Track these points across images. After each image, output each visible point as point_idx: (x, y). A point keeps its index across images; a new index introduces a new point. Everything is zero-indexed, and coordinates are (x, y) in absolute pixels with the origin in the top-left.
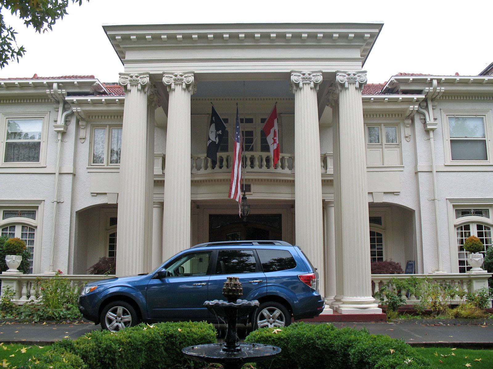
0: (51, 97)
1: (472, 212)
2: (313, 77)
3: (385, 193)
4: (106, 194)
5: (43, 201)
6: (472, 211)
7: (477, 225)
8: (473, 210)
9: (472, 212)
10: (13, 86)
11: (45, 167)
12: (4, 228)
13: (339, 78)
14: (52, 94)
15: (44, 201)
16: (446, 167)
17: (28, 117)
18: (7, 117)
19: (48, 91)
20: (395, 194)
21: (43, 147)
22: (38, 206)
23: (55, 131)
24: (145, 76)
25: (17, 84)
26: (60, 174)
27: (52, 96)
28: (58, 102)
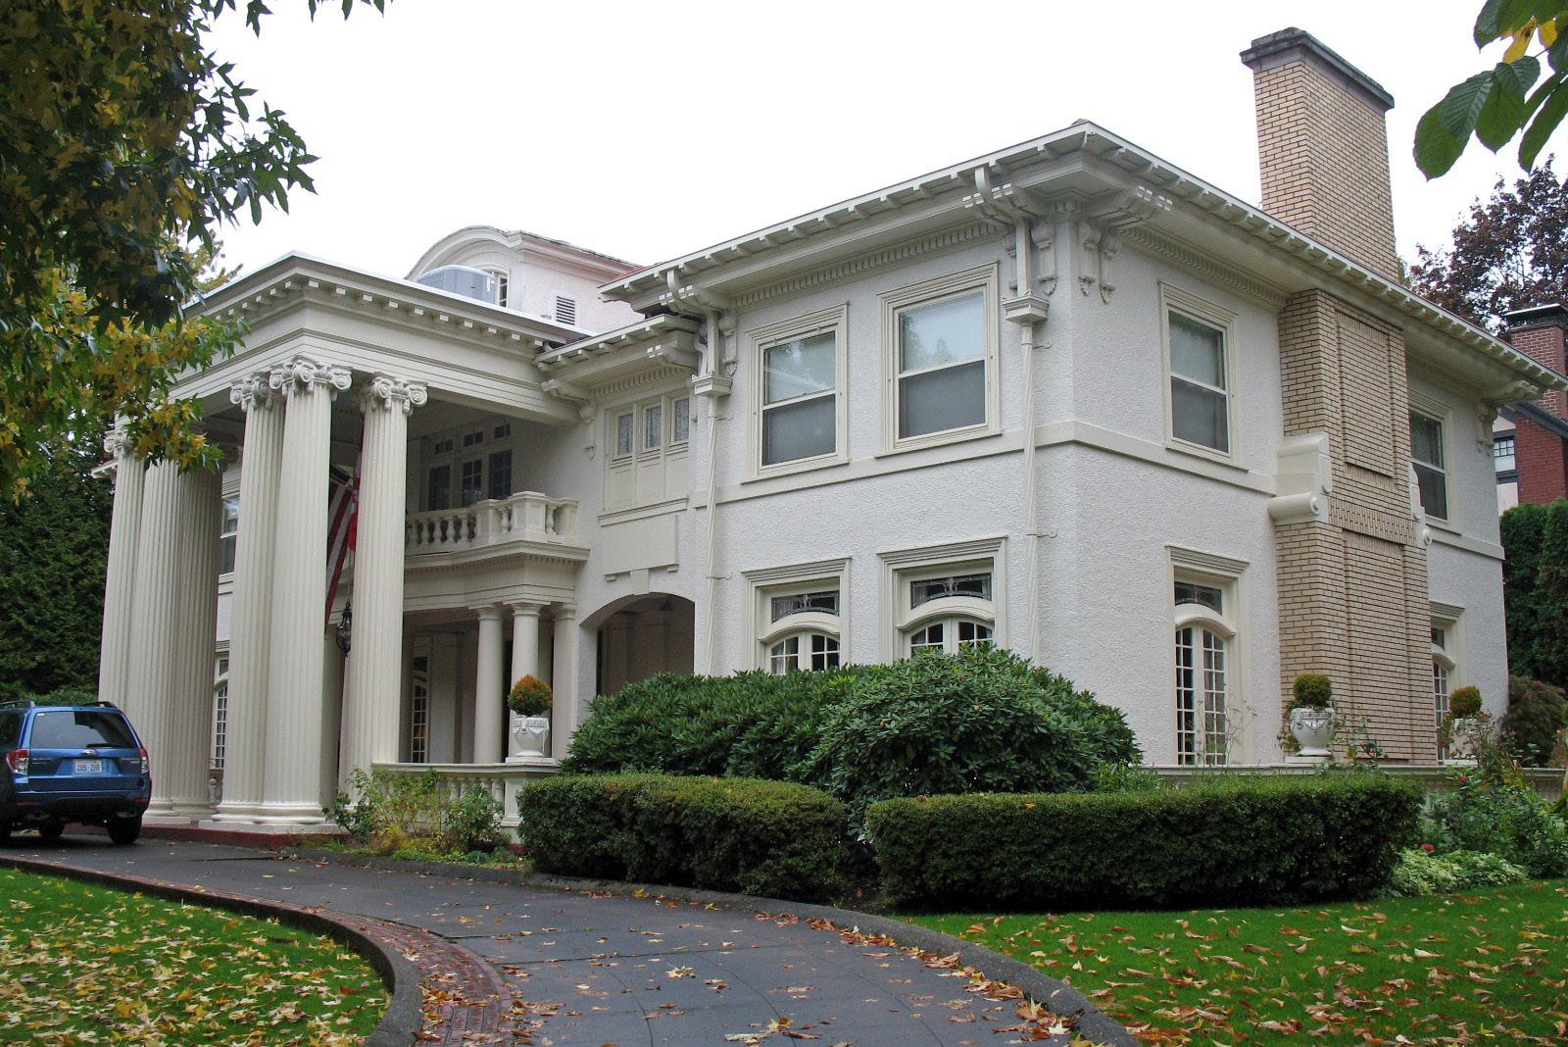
0: (1012, 207)
2: (334, 376)
3: (652, 570)
4: (628, 573)
5: (847, 562)
8: (954, 578)
10: (945, 188)
11: (847, 464)
12: (915, 633)
13: (378, 386)
14: (980, 206)
16: (880, 462)
17: (954, 289)
18: (895, 305)
22: (838, 577)
23: (1009, 319)
24: (344, 372)
25: (956, 179)
26: (1038, 448)
27: (985, 214)
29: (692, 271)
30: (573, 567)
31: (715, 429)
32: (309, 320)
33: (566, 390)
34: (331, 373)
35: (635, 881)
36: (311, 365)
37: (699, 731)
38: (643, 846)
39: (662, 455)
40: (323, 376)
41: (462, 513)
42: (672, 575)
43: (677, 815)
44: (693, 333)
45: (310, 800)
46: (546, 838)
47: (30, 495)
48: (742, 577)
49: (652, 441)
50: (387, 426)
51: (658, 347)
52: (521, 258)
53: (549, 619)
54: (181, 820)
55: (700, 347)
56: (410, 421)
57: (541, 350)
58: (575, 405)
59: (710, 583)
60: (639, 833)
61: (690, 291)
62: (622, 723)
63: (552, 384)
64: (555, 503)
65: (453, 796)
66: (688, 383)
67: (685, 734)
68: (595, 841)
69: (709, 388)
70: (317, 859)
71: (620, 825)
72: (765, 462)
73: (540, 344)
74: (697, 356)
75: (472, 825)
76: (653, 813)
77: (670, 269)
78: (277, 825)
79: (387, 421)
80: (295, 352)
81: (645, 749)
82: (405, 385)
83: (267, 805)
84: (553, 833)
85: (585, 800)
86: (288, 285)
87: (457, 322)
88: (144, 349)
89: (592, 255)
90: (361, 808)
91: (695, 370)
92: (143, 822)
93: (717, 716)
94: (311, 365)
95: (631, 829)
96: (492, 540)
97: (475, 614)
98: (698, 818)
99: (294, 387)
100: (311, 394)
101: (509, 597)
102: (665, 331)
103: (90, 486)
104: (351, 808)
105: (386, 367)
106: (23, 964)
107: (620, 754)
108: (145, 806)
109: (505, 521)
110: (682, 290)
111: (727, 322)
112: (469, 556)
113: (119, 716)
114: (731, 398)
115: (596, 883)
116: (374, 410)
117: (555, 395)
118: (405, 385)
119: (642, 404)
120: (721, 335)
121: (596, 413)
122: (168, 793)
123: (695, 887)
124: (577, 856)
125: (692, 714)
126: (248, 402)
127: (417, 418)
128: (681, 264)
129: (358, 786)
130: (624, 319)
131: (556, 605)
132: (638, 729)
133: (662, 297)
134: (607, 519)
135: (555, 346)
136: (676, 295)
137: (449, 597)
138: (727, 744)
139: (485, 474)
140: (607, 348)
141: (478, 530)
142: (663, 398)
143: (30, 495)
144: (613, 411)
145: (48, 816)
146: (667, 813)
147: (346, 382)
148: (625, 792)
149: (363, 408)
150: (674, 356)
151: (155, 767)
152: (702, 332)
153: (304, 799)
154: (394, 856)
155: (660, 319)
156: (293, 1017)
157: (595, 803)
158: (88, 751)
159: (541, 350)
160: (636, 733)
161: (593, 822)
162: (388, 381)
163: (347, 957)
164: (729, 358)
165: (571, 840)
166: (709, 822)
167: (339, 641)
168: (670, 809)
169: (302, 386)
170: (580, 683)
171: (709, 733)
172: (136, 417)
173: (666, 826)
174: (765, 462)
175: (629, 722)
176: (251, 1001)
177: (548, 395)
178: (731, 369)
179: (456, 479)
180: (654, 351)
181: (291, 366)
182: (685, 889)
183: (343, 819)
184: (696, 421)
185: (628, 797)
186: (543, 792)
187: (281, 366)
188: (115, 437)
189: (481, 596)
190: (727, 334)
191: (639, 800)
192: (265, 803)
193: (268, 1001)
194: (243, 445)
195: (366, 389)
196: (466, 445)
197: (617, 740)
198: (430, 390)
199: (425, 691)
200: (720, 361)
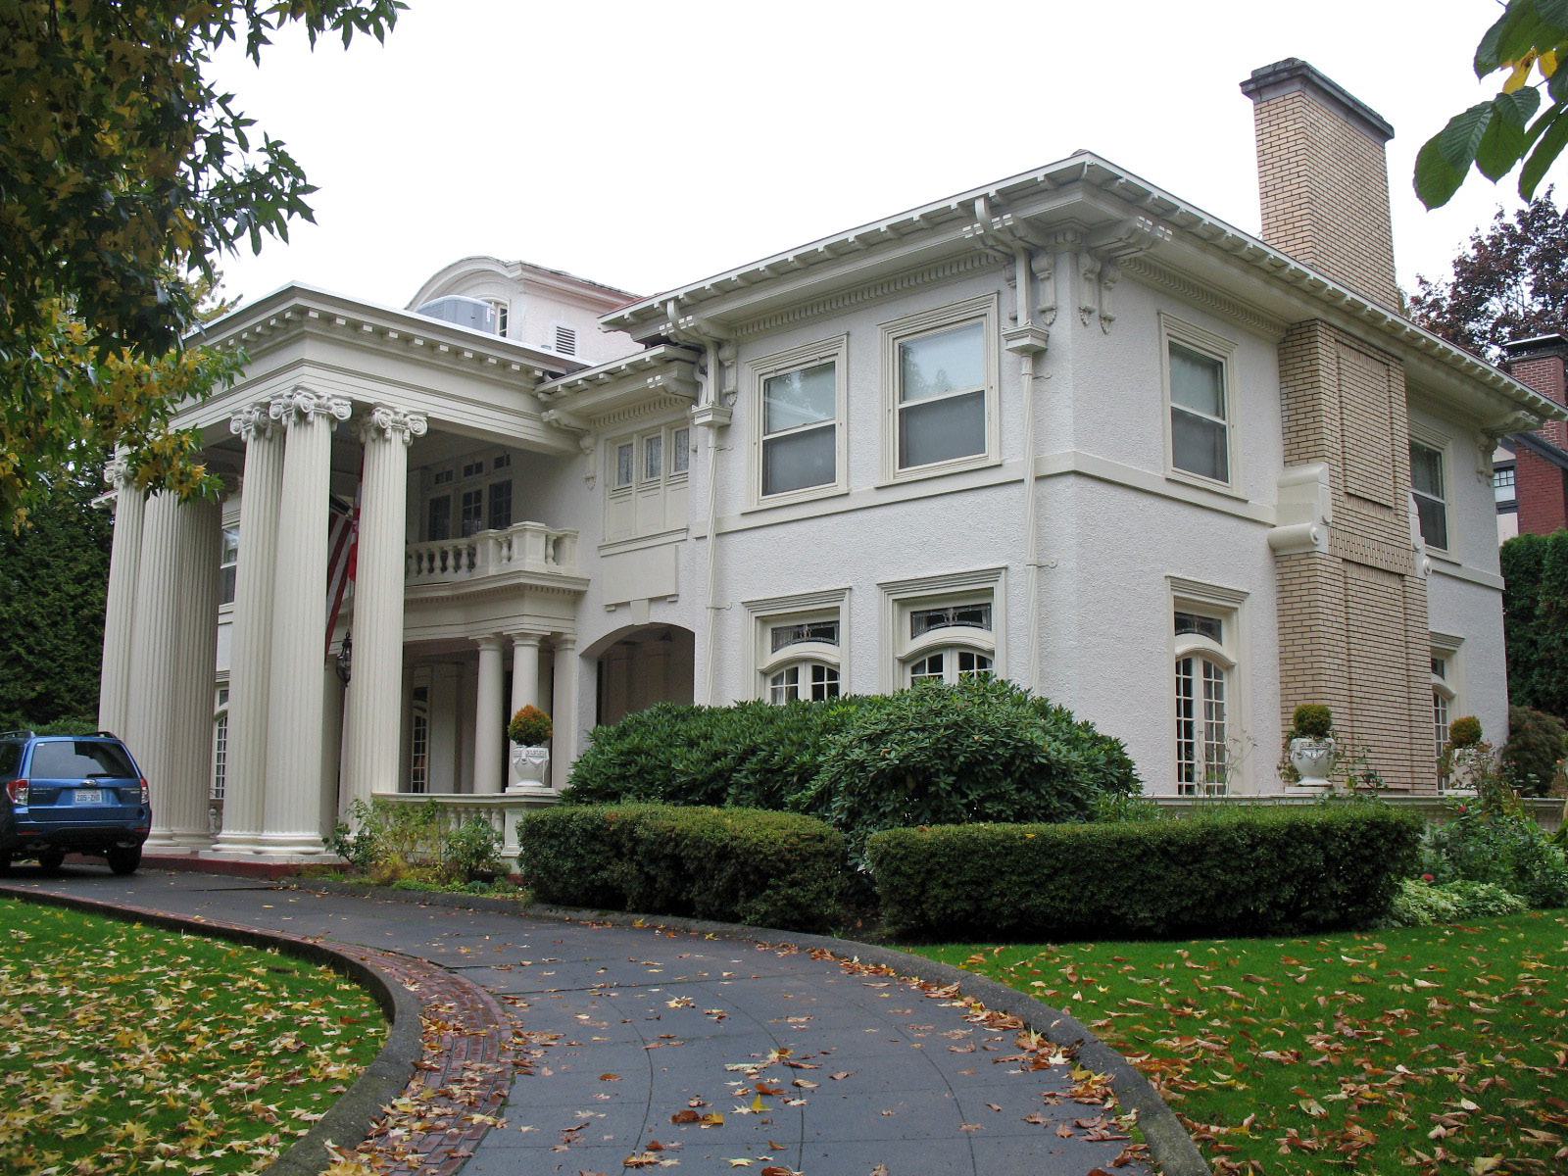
0: (1011, 238)
1: (951, 617)
3: (652, 600)
4: (628, 603)
5: (847, 592)
6: (951, 614)
7: (961, 655)
9: (951, 617)
13: (378, 416)
15: (1006, 568)
19: (967, 231)
20: (669, 599)
21: (991, 403)
23: (1009, 350)
26: (1038, 479)
28: (1011, 259)
29: (692, 301)
30: (573, 597)
32: (309, 351)
33: (566, 420)
34: (331, 403)
35: (635, 911)
36: (311, 395)
37: (699, 761)
40: (324, 407)
41: (462, 543)
42: (672, 606)
43: (677, 845)
44: (693, 363)
45: (310, 830)
46: (546, 868)
47: (30, 525)
49: (652, 471)
51: (658, 378)
52: (521, 288)
53: (549, 649)
55: (700, 377)
56: (410, 451)
57: (541, 380)
58: (575, 435)
59: (710, 613)
60: (639, 864)
62: (622, 753)
63: (552, 414)
64: (555, 533)
65: (453, 827)
67: (685, 764)
68: (595, 871)
69: (709, 418)
71: (620, 856)
72: (765, 492)
74: (697, 386)
75: (472, 855)
76: (653, 843)
77: (670, 300)
78: (277, 855)
82: (405, 416)
83: (267, 835)
84: (553, 863)
85: (584, 830)
87: (457, 352)
89: (592, 285)
90: (361, 838)
92: (143, 852)
93: (717, 746)
94: (311, 395)
96: (492, 571)
99: (294, 418)
100: (311, 424)
101: (510, 627)
102: (664, 362)
103: (90, 517)
104: (351, 838)
106: (23, 995)
107: (621, 784)
109: (505, 551)
110: (682, 321)
112: (477, 585)
113: (119, 746)
115: (596, 913)
116: (374, 441)
119: (642, 434)
120: (721, 365)
121: (596, 444)
122: (168, 823)
123: (695, 917)
125: (692, 744)
126: (248, 432)
127: (417, 449)
128: (681, 294)
130: (624, 349)
133: (662, 328)
135: (555, 376)
136: (676, 325)
137: (449, 627)
138: (727, 775)
140: (607, 378)
141: (478, 560)
143: (30, 525)
146: (667, 843)
147: (345, 412)
149: (362, 439)
150: (674, 387)
153: (304, 830)
154: (394, 886)
155: (660, 350)
156: (293, 1047)
157: (595, 833)
158: (88, 781)
159: (541, 380)
160: (636, 764)
161: (593, 852)
163: (347, 987)
164: (729, 389)
165: (571, 870)
167: (339, 672)
168: (670, 839)
169: (302, 416)
171: (709, 764)
173: (666, 856)
174: (765, 492)
175: (629, 752)
176: (251, 1031)
177: (548, 425)
178: (731, 400)
179: (455, 508)
184: (696, 451)
185: (628, 827)
186: (543, 822)
187: (281, 396)
188: (115, 467)
189: (482, 626)
193: (268, 1031)
195: (366, 419)
197: (617, 770)
198: (430, 420)
200: (720, 391)
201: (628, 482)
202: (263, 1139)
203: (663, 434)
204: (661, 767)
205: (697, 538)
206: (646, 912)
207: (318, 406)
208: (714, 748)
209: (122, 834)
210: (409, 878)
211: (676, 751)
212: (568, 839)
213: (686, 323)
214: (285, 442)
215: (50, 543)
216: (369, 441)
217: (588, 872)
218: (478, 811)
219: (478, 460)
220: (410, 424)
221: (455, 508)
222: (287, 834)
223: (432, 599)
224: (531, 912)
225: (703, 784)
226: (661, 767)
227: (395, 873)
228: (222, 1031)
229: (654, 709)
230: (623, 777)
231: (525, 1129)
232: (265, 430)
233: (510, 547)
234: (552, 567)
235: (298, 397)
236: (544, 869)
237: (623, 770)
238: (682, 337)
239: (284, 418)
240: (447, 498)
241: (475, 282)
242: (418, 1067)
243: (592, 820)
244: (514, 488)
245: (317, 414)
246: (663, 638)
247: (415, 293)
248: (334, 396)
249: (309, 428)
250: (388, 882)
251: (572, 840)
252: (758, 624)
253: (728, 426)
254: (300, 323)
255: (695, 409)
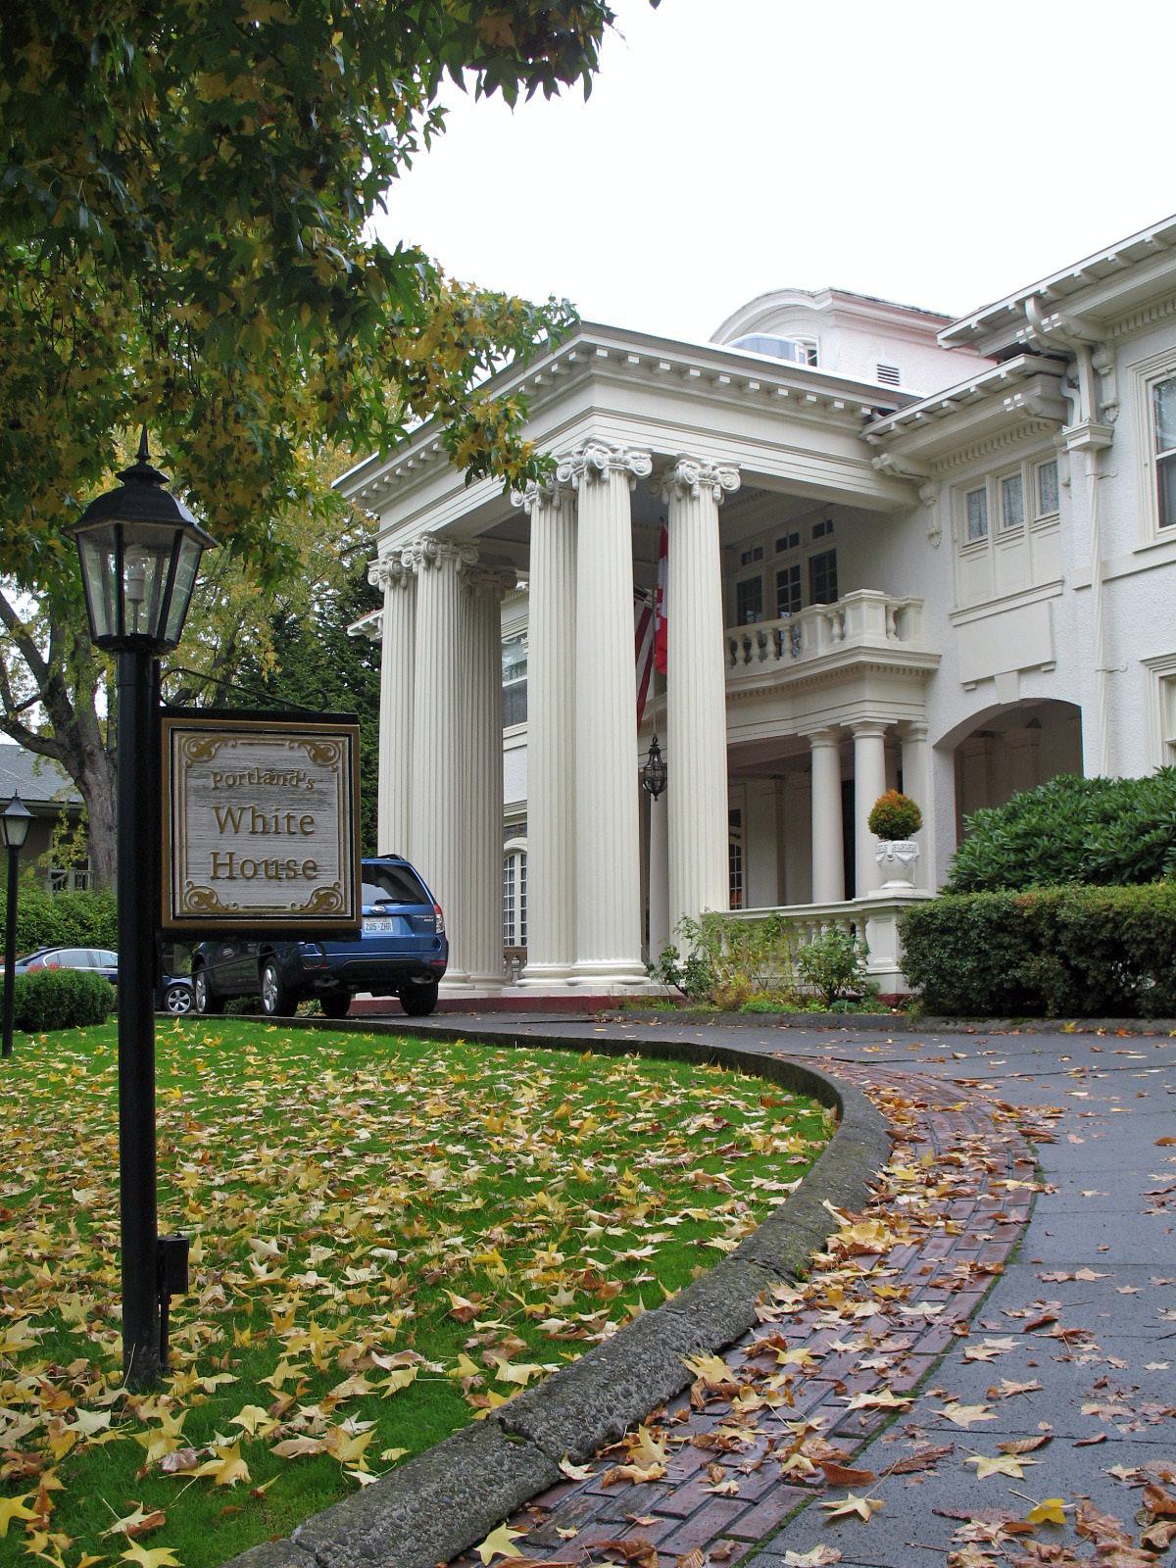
3: (1022, 672)
4: (991, 679)
13: (683, 470)
29: (1057, 296)
30: (922, 677)
31: (1096, 495)
32: (599, 397)
33: (903, 465)
34: (628, 457)
35: (1058, 1016)
36: (605, 449)
37: (1121, 838)
38: (1067, 974)
39: (1026, 532)
40: (620, 461)
41: (784, 622)
42: (1048, 675)
43: (1116, 928)
44: (1060, 376)
45: (632, 957)
46: (938, 970)
47: (279, 670)
48: (1142, 667)
49: (1011, 520)
50: (696, 518)
51: (1018, 397)
52: (832, 321)
53: (896, 741)
54: (479, 992)
55: (1069, 393)
56: (721, 510)
57: (869, 420)
58: (912, 485)
59: (1101, 677)
60: (1063, 956)
61: (1056, 321)
62: (1017, 836)
63: (886, 459)
64: (896, 602)
65: (802, 942)
66: (1056, 439)
67: (1099, 842)
68: (1003, 970)
69: (1086, 439)
70: (648, 1020)
71: (1036, 948)
72: (1163, 523)
73: (868, 412)
74: (1066, 404)
75: (833, 972)
76: (1083, 927)
77: (1028, 297)
78: (596, 986)
79: (696, 511)
80: (586, 435)
81: (1049, 865)
82: (714, 468)
83: (581, 964)
84: (947, 964)
85: (989, 920)
86: (572, 356)
87: (769, 390)
88: (466, 315)
89: (916, 312)
90: (692, 963)
91: (1065, 422)
92: (440, 997)
93: (1143, 816)
94: (605, 449)
95: (1052, 952)
96: (823, 651)
97: (805, 742)
98: (1148, 927)
99: (586, 477)
100: (606, 482)
101: (847, 717)
102: (1024, 377)
103: (342, 658)
104: (680, 965)
105: (694, 448)
106: (355, 1093)
107: (1019, 873)
108: (438, 973)
109: (836, 629)
110: (1045, 321)
111: (1102, 358)
112: (805, 669)
113: (407, 869)
114: (1114, 449)
115: (1008, 1022)
116: (679, 500)
117: (890, 473)
118: (714, 468)
119: (995, 474)
120: (1096, 374)
121: (939, 491)
122: (462, 965)
123: (1142, 1017)
124: (980, 991)
125: (1107, 819)
126: (532, 502)
127: (731, 507)
128: (1042, 288)
129: (689, 937)
130: (968, 372)
131: (904, 724)
132: (1039, 842)
133: (1020, 333)
134: (959, 617)
135: (885, 413)
136: (1038, 329)
137: (774, 724)
138: (1158, 851)
139: (805, 583)
140: (953, 406)
141: (805, 642)
142: (1023, 465)
143: (279, 670)
144: (957, 487)
145: (336, 982)
146: (1103, 926)
147: (645, 467)
148: (1043, 905)
149: (665, 499)
150: (1038, 407)
151: (449, 925)
152: (1071, 374)
153: (624, 956)
154: (741, 1010)
155: (1019, 361)
156: (714, 1126)
157: (1000, 924)
158: (377, 908)
159: (869, 420)
160: (1036, 848)
161: (1000, 946)
162: (694, 464)
163: (747, 1078)
164: (1108, 401)
165: (971, 971)
166: (1164, 931)
167: (654, 783)
168: (1107, 920)
169: (595, 473)
170: (937, 816)
171: (1134, 839)
172: (452, 422)
173: (1101, 942)
174: (1163, 523)
175: (1026, 834)
176: (650, 1115)
177: (882, 474)
178: (1111, 415)
179: (769, 592)
180: (1014, 403)
181: (581, 453)
182: (1131, 1020)
183: (671, 977)
184: (1067, 485)
185: (1047, 913)
186: (932, 915)
187: (569, 454)
188: (380, 567)
189: (812, 719)
190: (1103, 372)
191: (1063, 913)
192: (579, 962)
193: (673, 1115)
194: (527, 569)
195: (668, 475)
196: (778, 551)
197: (1012, 857)
198: (743, 473)
199: (739, 849)
200: (1097, 406)
201: (981, 534)
202: (727, 1207)
203: (1023, 471)
204: (1068, 849)
205: (1078, 589)
206: (1072, 1016)
207: (614, 461)
208: (1140, 819)
209: (420, 969)
210: (754, 1000)
211: (1089, 828)
212: (966, 933)
213: (1052, 323)
214: (576, 511)
215: (301, 689)
216: (674, 501)
217: (995, 972)
218: (832, 923)
219: (792, 532)
220: (720, 480)
221: (769, 592)
222: (605, 961)
223: (751, 692)
224: (921, 1027)
225: (1127, 865)
226: (1068, 849)
227: (741, 994)
228: (613, 1115)
229: (1051, 784)
230: (1022, 865)
231: (1088, 1193)
232: (552, 498)
233: (842, 623)
234: (895, 644)
235: (590, 451)
236: (935, 973)
237: (1021, 856)
238: (1046, 343)
239: (574, 479)
240: (757, 581)
241: (779, 320)
242: (897, 1139)
243: (997, 907)
244: (838, 558)
245: (613, 471)
246: (1029, 726)
247: (718, 326)
248: (632, 449)
249: (605, 488)
250: (734, 1006)
251: (973, 934)
252: (1164, 684)
253: (1110, 447)
254: (587, 366)
255: (1066, 430)
